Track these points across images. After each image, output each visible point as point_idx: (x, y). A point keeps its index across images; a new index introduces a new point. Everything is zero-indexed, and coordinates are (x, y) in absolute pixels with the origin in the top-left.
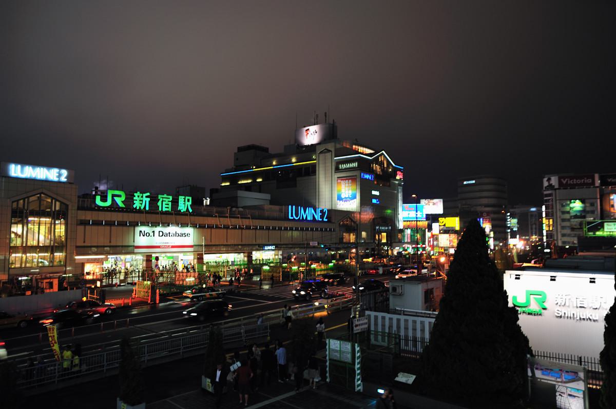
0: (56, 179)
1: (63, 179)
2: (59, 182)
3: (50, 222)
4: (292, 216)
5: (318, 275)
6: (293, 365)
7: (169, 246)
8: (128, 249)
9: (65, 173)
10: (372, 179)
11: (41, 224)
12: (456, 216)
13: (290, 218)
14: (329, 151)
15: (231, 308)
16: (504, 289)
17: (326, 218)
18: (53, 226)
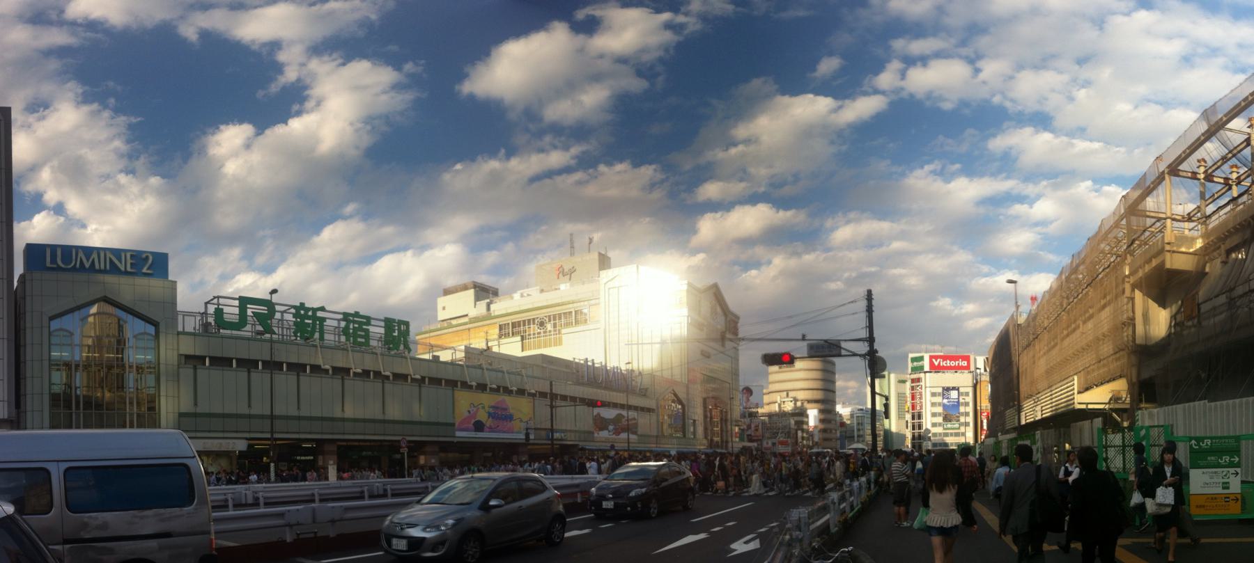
6: (32, 231)
7: (920, 417)
8: (880, 411)
12: (604, 509)
13: (48, 265)
16: (875, 348)
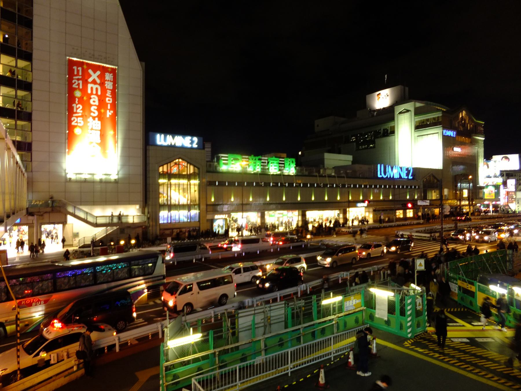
0: (189, 146)
1: (195, 146)
2: (192, 148)
3: (186, 184)
4: (381, 174)
5: (360, 258)
9: (195, 139)
10: (454, 136)
11: (172, 186)
13: (379, 176)
14: (408, 111)
15: (387, 273)
17: (411, 176)
18: (189, 186)
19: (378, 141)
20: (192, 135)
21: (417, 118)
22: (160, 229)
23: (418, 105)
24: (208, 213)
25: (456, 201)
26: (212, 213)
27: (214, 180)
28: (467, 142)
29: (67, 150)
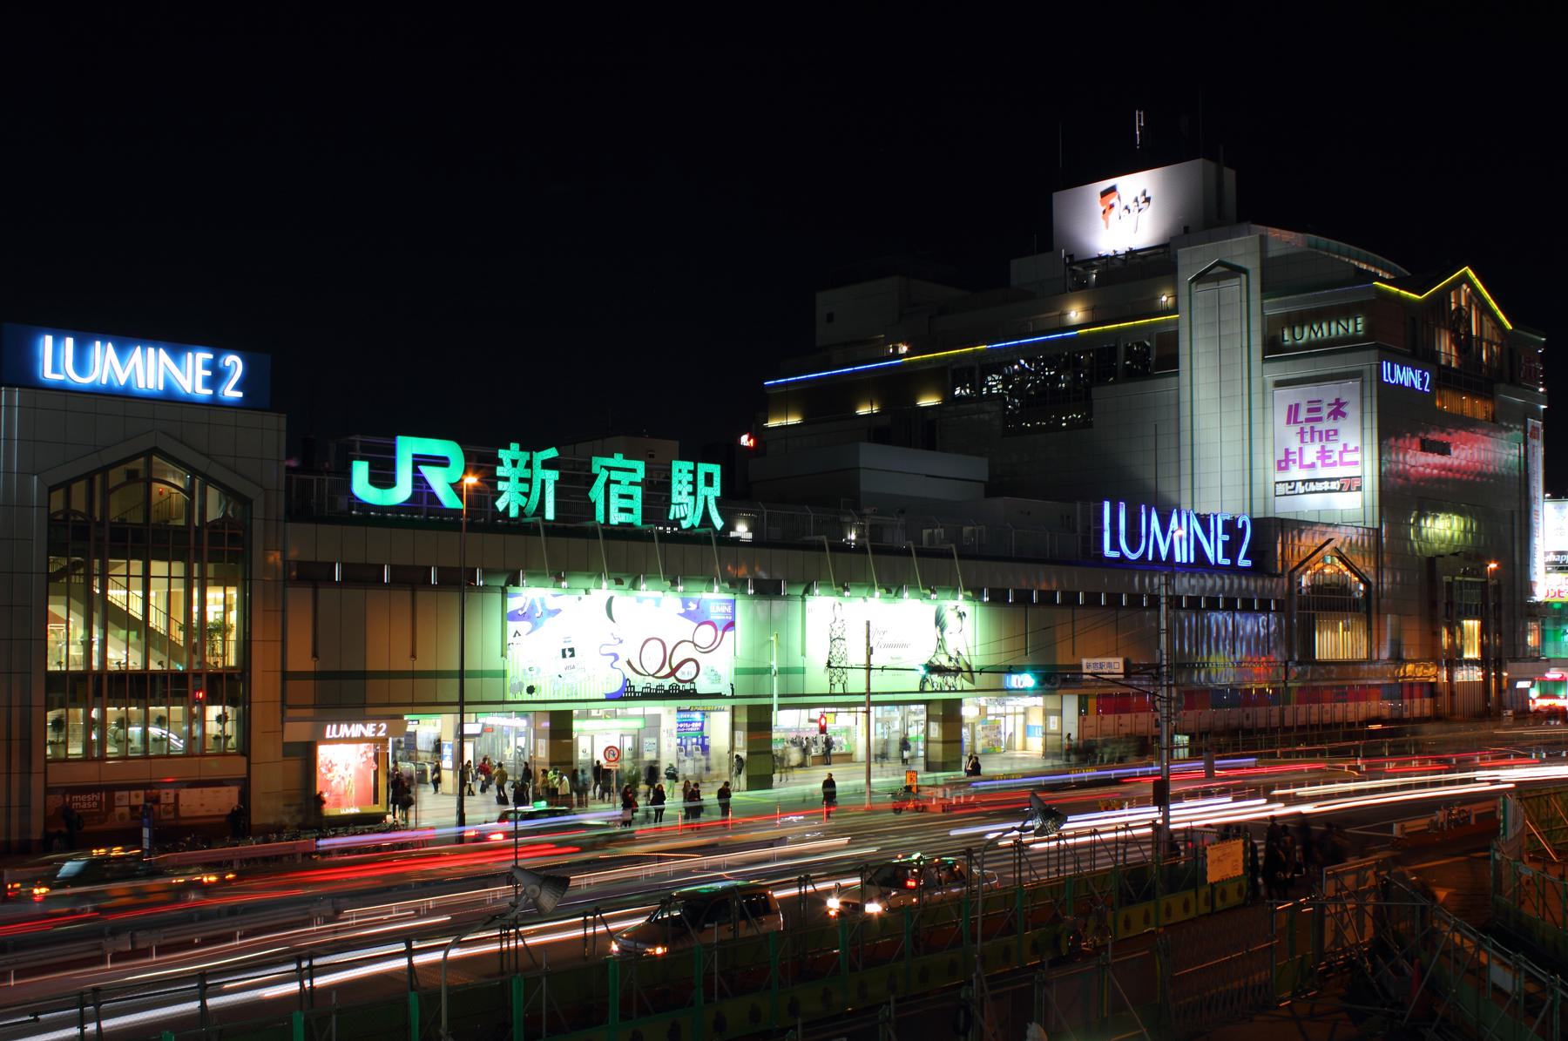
1: (230, 392)
2: (215, 404)
4: (1115, 545)
9: (234, 363)
13: (1108, 552)
14: (1236, 271)
19: (1103, 396)
20: (219, 345)
21: (1272, 306)
22: (48, 790)
23: (1284, 240)
24: (290, 713)
25: (1432, 670)
26: (309, 712)
27: (419, 562)
28: (1481, 415)
29: (1039, 671)
